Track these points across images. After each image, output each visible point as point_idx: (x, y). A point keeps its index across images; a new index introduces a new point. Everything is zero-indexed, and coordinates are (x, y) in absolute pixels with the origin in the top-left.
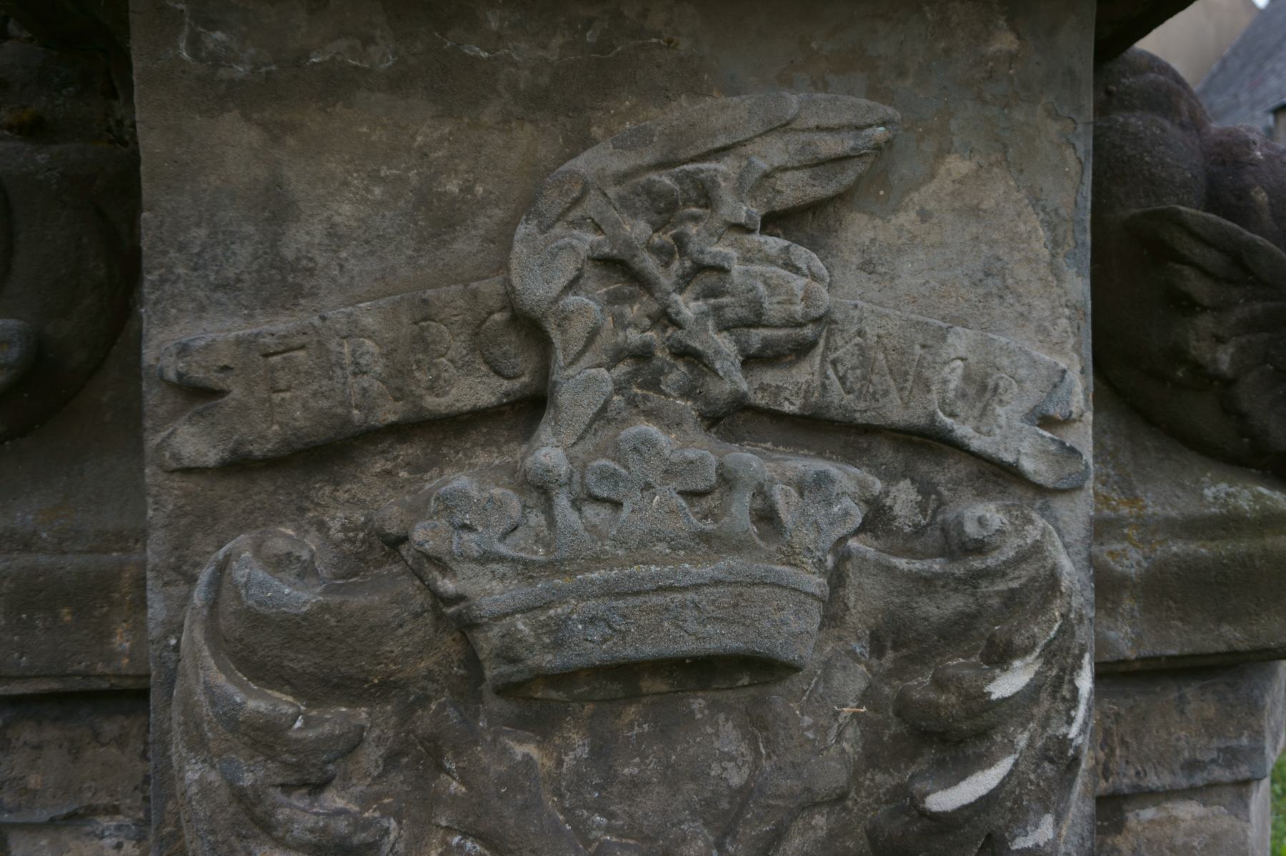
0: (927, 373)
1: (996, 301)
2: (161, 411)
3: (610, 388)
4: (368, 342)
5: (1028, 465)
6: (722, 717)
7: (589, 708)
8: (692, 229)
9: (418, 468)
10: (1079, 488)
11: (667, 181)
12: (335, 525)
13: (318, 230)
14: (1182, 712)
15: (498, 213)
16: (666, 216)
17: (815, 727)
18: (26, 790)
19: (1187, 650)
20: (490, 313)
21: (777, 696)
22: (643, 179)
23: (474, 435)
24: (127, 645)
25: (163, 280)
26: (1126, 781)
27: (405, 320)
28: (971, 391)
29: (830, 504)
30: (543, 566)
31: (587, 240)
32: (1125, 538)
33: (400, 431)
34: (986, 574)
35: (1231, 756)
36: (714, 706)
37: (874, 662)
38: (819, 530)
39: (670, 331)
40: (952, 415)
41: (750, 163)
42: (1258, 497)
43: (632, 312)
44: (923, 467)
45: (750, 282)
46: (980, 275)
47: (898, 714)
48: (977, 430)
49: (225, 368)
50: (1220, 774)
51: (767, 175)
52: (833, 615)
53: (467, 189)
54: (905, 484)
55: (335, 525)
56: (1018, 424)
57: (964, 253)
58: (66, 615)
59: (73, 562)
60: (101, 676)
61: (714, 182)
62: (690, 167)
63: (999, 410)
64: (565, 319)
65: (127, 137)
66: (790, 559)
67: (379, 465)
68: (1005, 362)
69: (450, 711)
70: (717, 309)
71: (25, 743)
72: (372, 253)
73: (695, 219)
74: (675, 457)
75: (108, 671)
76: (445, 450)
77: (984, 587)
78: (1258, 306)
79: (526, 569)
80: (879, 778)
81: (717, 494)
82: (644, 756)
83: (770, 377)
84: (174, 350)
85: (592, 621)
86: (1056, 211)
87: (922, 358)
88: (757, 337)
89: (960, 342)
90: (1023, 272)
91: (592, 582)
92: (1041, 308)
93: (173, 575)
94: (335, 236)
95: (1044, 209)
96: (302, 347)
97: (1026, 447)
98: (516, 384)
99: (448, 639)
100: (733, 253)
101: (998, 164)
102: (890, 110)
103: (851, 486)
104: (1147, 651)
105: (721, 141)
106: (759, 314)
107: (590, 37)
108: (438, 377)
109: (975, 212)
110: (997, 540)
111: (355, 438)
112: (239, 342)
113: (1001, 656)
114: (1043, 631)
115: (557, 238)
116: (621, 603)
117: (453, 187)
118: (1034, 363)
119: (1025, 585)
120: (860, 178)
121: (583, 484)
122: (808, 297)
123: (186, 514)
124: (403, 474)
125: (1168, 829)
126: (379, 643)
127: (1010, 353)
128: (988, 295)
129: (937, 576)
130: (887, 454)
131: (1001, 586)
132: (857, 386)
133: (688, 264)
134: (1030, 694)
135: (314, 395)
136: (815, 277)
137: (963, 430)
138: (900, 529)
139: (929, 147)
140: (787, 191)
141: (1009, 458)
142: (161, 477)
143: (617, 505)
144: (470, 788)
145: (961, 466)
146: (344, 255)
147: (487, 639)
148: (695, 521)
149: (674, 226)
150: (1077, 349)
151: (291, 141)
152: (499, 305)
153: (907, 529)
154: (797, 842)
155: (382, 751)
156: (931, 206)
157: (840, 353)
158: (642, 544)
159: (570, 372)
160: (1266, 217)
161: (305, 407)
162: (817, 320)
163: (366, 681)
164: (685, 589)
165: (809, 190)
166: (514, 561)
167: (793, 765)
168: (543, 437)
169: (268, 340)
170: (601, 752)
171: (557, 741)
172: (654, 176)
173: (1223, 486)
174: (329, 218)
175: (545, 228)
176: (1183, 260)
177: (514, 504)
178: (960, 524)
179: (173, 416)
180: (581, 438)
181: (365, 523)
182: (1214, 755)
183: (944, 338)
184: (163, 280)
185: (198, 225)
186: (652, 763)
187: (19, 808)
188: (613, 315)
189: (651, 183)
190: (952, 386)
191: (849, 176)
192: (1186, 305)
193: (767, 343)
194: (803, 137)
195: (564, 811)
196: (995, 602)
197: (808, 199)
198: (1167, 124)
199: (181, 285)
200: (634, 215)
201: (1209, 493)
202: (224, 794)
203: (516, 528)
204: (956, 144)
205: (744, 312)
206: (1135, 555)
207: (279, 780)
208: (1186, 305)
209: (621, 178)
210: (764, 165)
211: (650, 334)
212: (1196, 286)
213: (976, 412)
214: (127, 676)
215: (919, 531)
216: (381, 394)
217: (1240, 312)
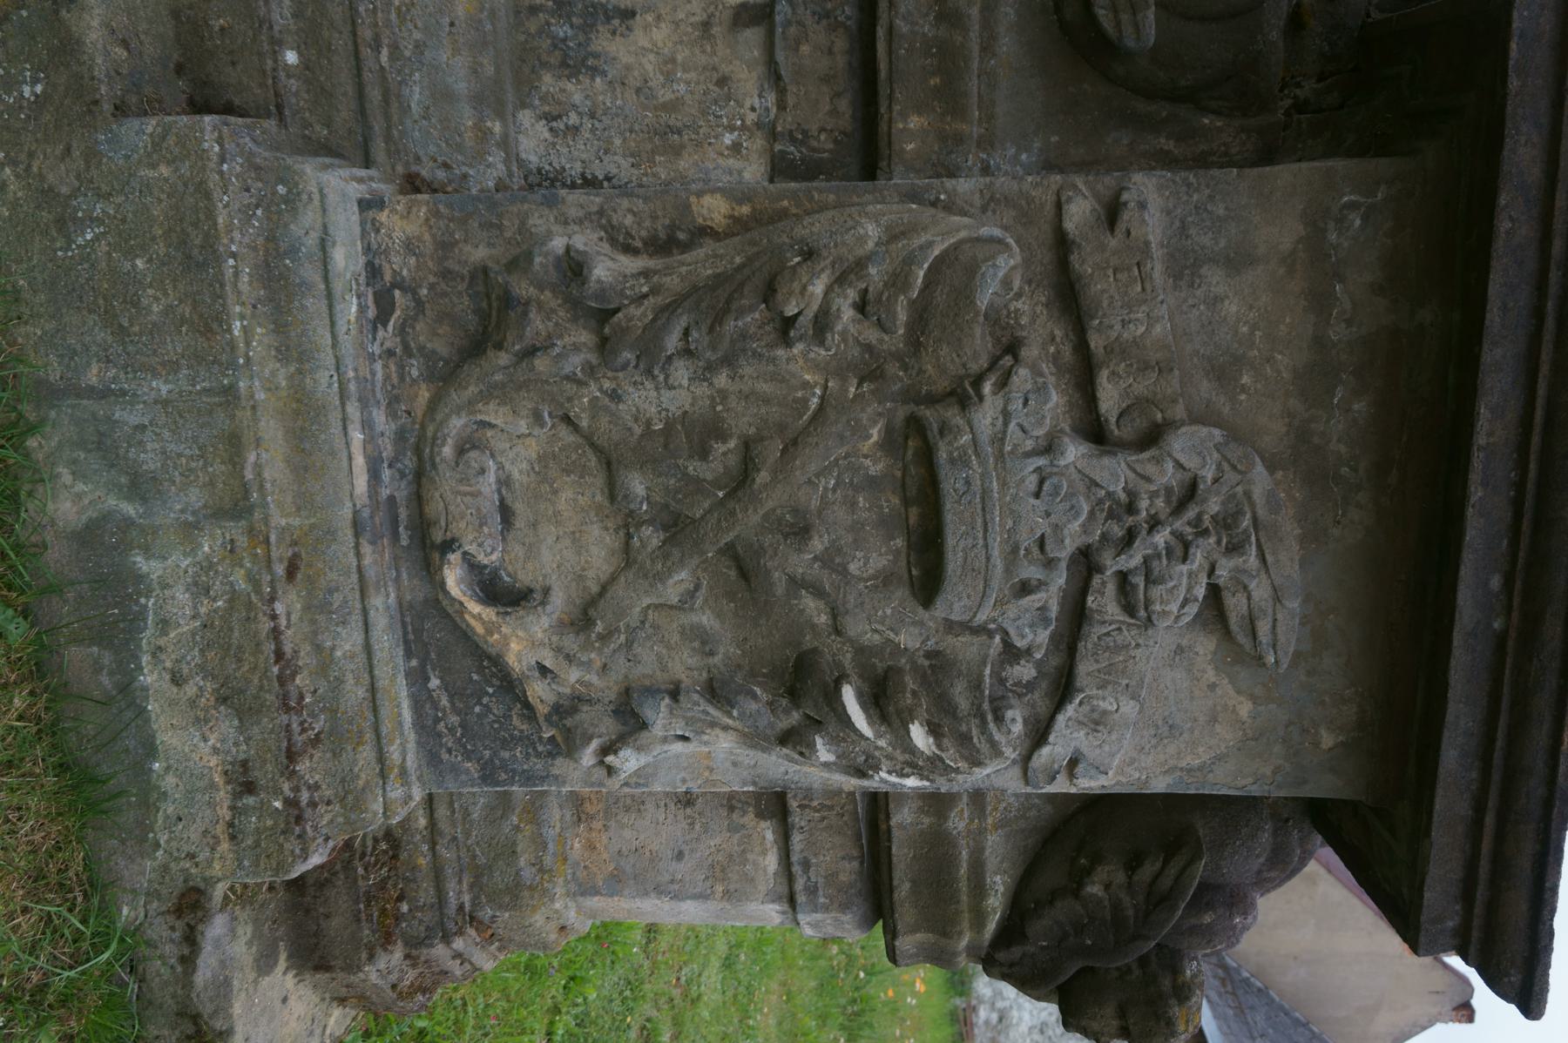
0: (1110, 688)
1: (1153, 732)
2: (1099, 187)
3: (1111, 489)
4: (1143, 329)
5: (1045, 751)
6: (891, 558)
7: (899, 474)
8: (1212, 540)
9: (1055, 359)
10: (1027, 783)
11: (1245, 524)
12: (1019, 305)
13: (1220, 290)
14: (843, 858)
15: (1226, 410)
16: (1222, 523)
17: (885, 616)
18: (798, 43)
19: (895, 859)
20: (1162, 411)
21: (901, 593)
22: (1246, 508)
23: (1077, 395)
24: (912, 125)
25: (1189, 185)
26: (797, 820)
27: (1159, 355)
28: (1095, 716)
29: (1031, 627)
30: (1001, 451)
31: (1209, 474)
32: (972, 820)
33: (1082, 347)
34: (984, 722)
35: (812, 891)
36: (897, 552)
37: (922, 653)
38: (1015, 620)
39: (1145, 526)
40: (1081, 703)
41: (1254, 577)
42: (994, 910)
43: (1160, 502)
44: (1044, 685)
45: (1176, 576)
46: (1170, 722)
47: (890, 668)
48: (1070, 719)
49: (1128, 233)
50: (800, 884)
51: (1245, 587)
52: (950, 626)
53: (1244, 389)
54: (1034, 673)
55: (1019, 305)
56: (1073, 745)
57: (1186, 712)
58: (935, 81)
59: (973, 85)
60: (890, 107)
61: (1243, 554)
62: (1253, 538)
63: (1082, 733)
64: (1158, 461)
65: (1286, 92)
66: (1000, 603)
67: (1058, 333)
68: (1114, 737)
69: (899, 385)
70: (1159, 556)
71: (833, 42)
72: (1203, 326)
73: (1219, 542)
74: (1066, 532)
75: (895, 114)
76: (1067, 376)
77: (974, 722)
78: (1131, 912)
79: (999, 439)
80: (849, 656)
81: (1041, 557)
82: (869, 510)
83: (1111, 588)
84: (1142, 199)
85: (968, 482)
86: (1211, 771)
87: (1120, 684)
88: (1139, 581)
89: (1129, 708)
90: (1172, 749)
91: (991, 482)
92: (1147, 761)
93: (987, 197)
94: (1215, 301)
95: (1213, 763)
96: (1143, 289)
97: (1059, 749)
98: (1113, 427)
99: (946, 383)
100: (1195, 566)
101: (1245, 734)
102: (1285, 666)
103: (1039, 640)
104: (896, 833)
105: (1269, 558)
106: (1154, 582)
107: (1345, 470)
108: (1121, 377)
109: (1213, 719)
110: (1004, 729)
111: (1079, 318)
112: (1147, 243)
113: (934, 730)
114: (950, 757)
115: (1211, 455)
116: (978, 500)
117: (1245, 379)
118: (1113, 755)
119: (974, 746)
120: (1241, 646)
121: (1051, 475)
122: (1165, 613)
123: (1028, 204)
124: (1052, 349)
125: (758, 849)
126: (948, 344)
127: (1119, 740)
128: (1157, 727)
129: (982, 692)
130: (1055, 661)
131: (975, 732)
132: (1102, 643)
133: (1190, 538)
134: (911, 749)
135: (1112, 297)
136: (1178, 618)
137: (1070, 710)
138: (1004, 669)
139: (1258, 691)
140: (1234, 600)
141: (1051, 739)
142: (1054, 187)
143: (1037, 495)
144: (853, 401)
145: (1044, 708)
146: (1202, 307)
147: (955, 415)
148: (1026, 544)
149: (1214, 528)
150: (1118, 783)
151: (1282, 271)
152: (1167, 416)
153: (1004, 674)
154: (812, 605)
155: (874, 342)
156: (1219, 692)
157: (1126, 632)
158: (1012, 512)
159: (1123, 464)
160: (1193, 921)
161: (1103, 291)
162: (1149, 619)
163: (922, 333)
164: (985, 539)
165: (1234, 614)
166: (1005, 432)
167: (862, 603)
168: (1081, 448)
169: (1149, 266)
170: (873, 483)
171: (878, 454)
172: (1248, 516)
173: (1001, 889)
174: (1228, 297)
175: (1217, 447)
176: (1166, 862)
177: (1041, 432)
178: (1011, 707)
179: (1096, 195)
180: (1079, 471)
181: (1020, 325)
182: (813, 879)
183: (1133, 698)
184: (1189, 185)
185: (1226, 208)
186: (865, 515)
187: (785, 39)
188: (1158, 491)
189: (1244, 514)
190: (1101, 703)
191: (1242, 639)
192: (1133, 864)
193: (1135, 587)
194: (1270, 611)
195: (837, 460)
196: (964, 728)
197: (1228, 613)
198: (1262, 860)
199: (1185, 198)
200: (1223, 503)
201: (998, 878)
202: (860, 252)
203: (1024, 431)
204: (1260, 708)
205: (1156, 573)
206: (961, 826)
207: (871, 289)
208: (1133, 864)
209: (1248, 495)
210: (1252, 586)
211: (1144, 514)
213: (1081, 718)
214: (890, 128)
215: (1002, 681)
216: (1108, 337)
217: (1126, 900)
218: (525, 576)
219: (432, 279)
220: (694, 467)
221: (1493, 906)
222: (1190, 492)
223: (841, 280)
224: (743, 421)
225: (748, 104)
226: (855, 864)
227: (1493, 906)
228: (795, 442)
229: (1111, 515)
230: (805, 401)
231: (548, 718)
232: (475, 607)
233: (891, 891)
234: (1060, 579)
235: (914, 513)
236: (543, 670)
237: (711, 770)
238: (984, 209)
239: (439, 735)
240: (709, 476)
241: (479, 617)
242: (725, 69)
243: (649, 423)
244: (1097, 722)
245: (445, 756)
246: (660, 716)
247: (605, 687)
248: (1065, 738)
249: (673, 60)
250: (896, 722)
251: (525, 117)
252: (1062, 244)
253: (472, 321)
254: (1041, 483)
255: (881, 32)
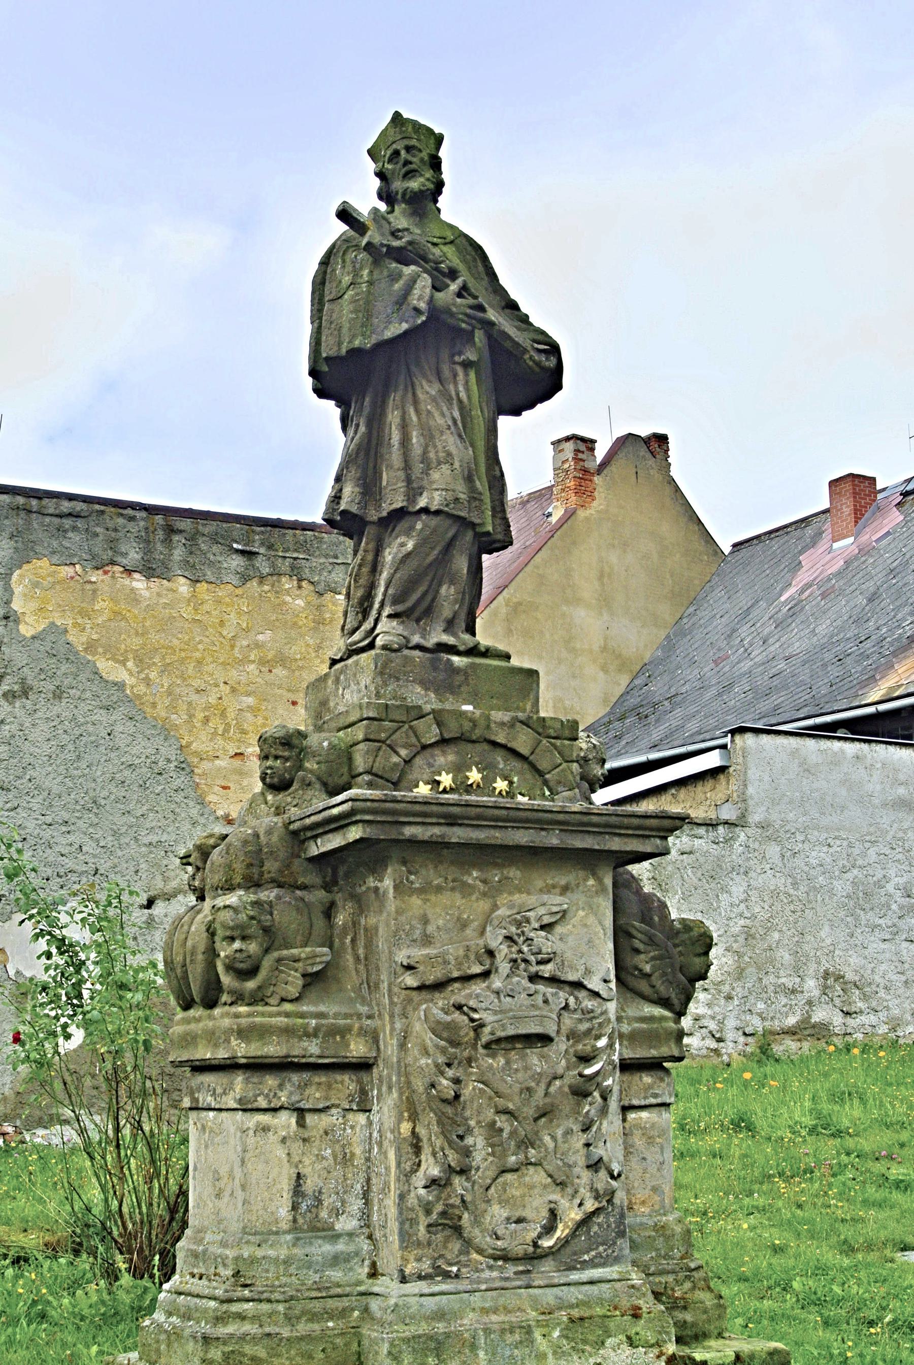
5: (601, 992)
8: (525, 929)
13: (435, 927)
15: (476, 923)
34: (594, 1017)
44: (576, 993)
53: (468, 917)
77: (594, 1021)
79: (495, 1013)
83: (542, 967)
88: (540, 956)
113: (598, 1037)
117: (465, 916)
130: (567, 988)
137: (585, 983)
143: (513, 997)
162: (554, 953)
176: (635, 938)
179: (403, 974)
193: (542, 959)
196: (596, 1025)
201: (646, 1010)
202: (432, 1066)
209: (509, 916)
212: (637, 944)
218: (545, 1213)
219: (431, 1251)
220: (505, 1135)
221: (651, 829)
222: (509, 938)
223: (442, 1073)
224: (490, 1114)
225: (335, 1122)
226: (643, 1075)
227: (651, 829)
228: (496, 1093)
229: (518, 968)
230: (480, 1089)
231: (600, 1202)
232: (558, 1233)
233: (655, 1058)
234: (541, 987)
235: (518, 1046)
236: (580, 1205)
237: (615, 1133)
238: (407, 1018)
239: (607, 1256)
240: (509, 1128)
241: (563, 1231)
242: (321, 1132)
243: (488, 1154)
244: (588, 972)
245: (616, 1254)
246: (599, 1151)
247: (586, 1176)
248: (594, 983)
249: (317, 1155)
250: (596, 1053)
251: (338, 1227)
252: (420, 988)
253: (448, 1232)
254: (509, 996)
255: (320, 1061)
